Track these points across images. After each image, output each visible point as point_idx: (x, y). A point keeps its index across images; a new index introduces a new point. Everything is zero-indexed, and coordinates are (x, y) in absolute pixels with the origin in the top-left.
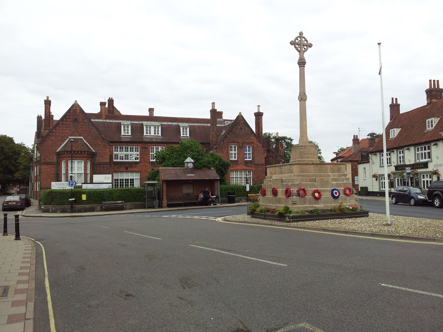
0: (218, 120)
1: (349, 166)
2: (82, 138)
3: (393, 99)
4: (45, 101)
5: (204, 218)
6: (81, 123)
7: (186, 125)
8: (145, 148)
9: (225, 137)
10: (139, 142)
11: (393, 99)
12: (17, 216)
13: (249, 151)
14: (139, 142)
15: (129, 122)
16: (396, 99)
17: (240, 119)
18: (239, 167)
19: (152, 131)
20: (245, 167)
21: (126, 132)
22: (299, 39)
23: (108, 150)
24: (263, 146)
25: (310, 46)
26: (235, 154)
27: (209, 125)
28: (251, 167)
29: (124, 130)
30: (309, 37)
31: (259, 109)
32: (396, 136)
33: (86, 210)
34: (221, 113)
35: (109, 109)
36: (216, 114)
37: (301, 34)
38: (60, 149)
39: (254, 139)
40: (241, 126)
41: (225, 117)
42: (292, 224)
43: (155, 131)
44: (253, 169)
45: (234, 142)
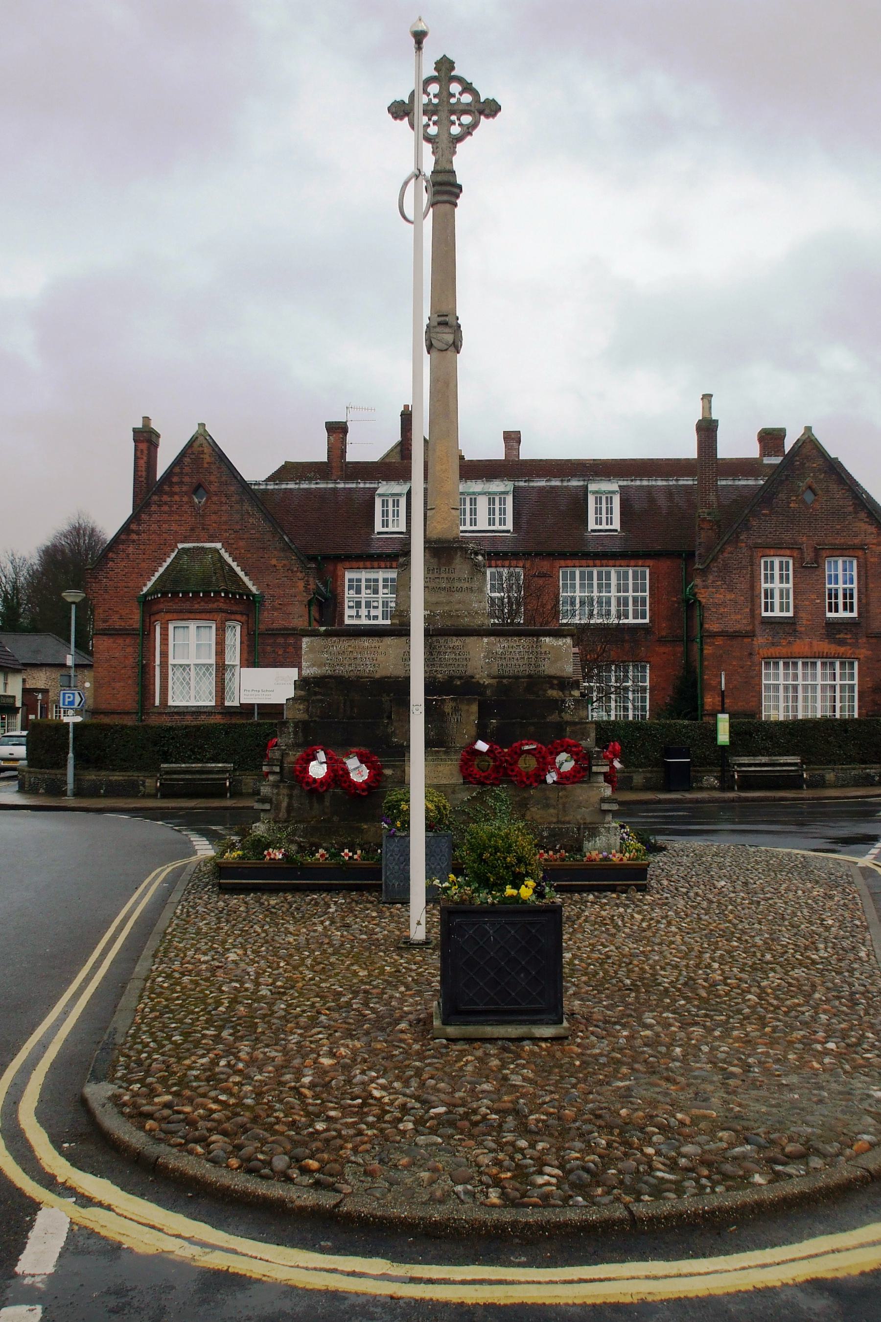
2: (218, 545)
4: (136, 431)
6: (215, 499)
15: (613, 486)
18: (801, 646)
20: (825, 647)
28: (855, 645)
38: (149, 584)
40: (809, 480)
43: (491, 511)
44: (863, 652)
45: (777, 547)
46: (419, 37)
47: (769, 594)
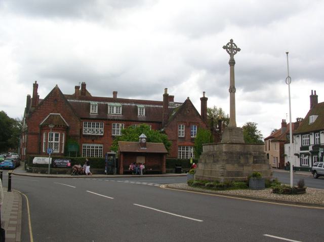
0: (170, 102)
1: (278, 145)
2: (60, 114)
3: (312, 91)
5: (151, 184)
7: (142, 106)
8: (108, 124)
9: (175, 117)
10: (104, 119)
11: (312, 91)
12: (10, 174)
13: (183, 129)
14: (104, 119)
15: (96, 103)
16: (315, 91)
17: (188, 102)
19: (115, 110)
21: (94, 111)
22: (230, 44)
23: (79, 124)
24: (207, 127)
25: (239, 50)
26: (183, 132)
27: (162, 107)
29: (93, 109)
30: (238, 43)
31: (204, 95)
32: (314, 121)
33: (60, 173)
34: (172, 98)
35: (82, 91)
36: (168, 98)
37: (232, 41)
38: (42, 123)
39: (199, 120)
41: (175, 100)
42: (219, 192)
43: (117, 110)
46: (287, 53)
47: (180, 132)
